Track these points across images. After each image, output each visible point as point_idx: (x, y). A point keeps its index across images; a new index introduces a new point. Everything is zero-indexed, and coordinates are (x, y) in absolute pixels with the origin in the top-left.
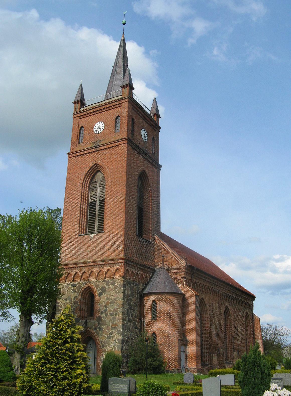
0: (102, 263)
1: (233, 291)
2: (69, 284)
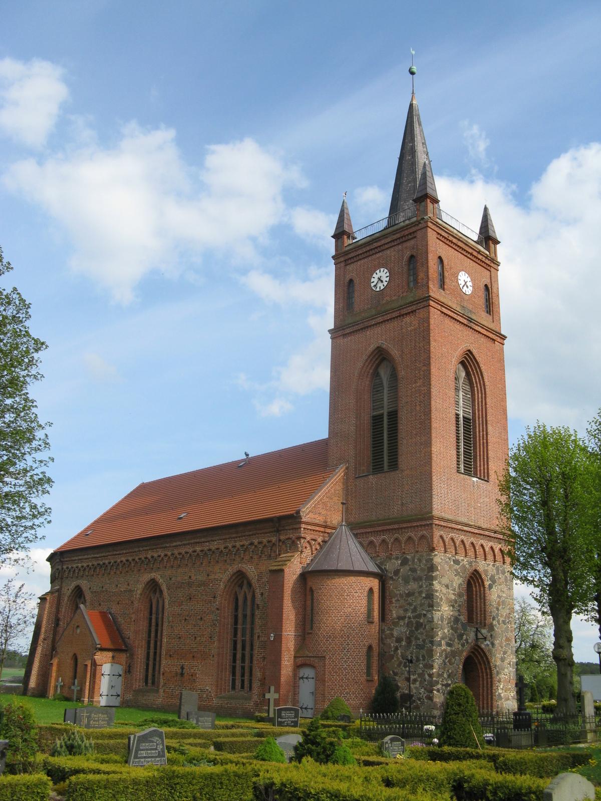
0: (492, 535)
2: (450, 559)
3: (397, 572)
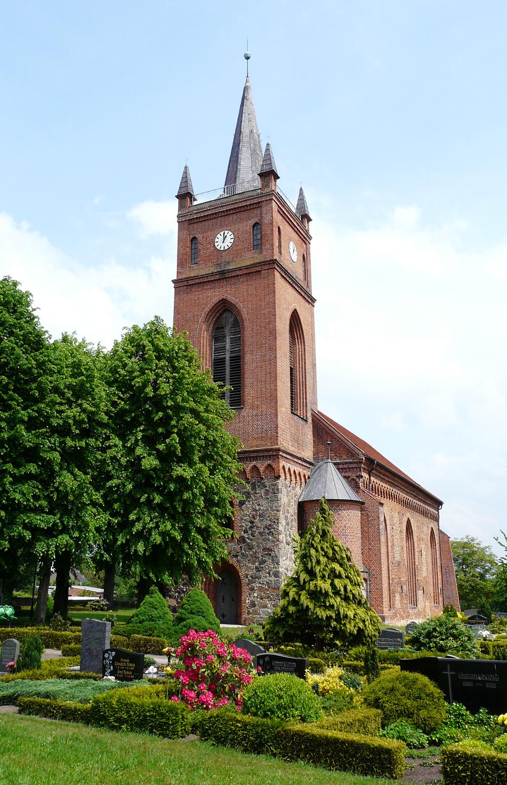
1: (415, 495)
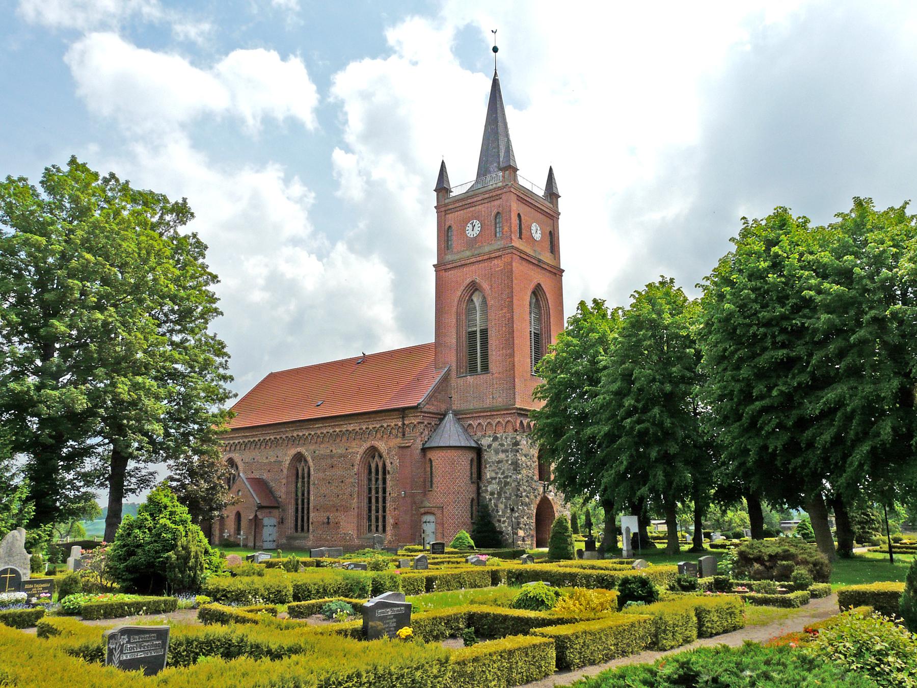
3: (490, 446)
